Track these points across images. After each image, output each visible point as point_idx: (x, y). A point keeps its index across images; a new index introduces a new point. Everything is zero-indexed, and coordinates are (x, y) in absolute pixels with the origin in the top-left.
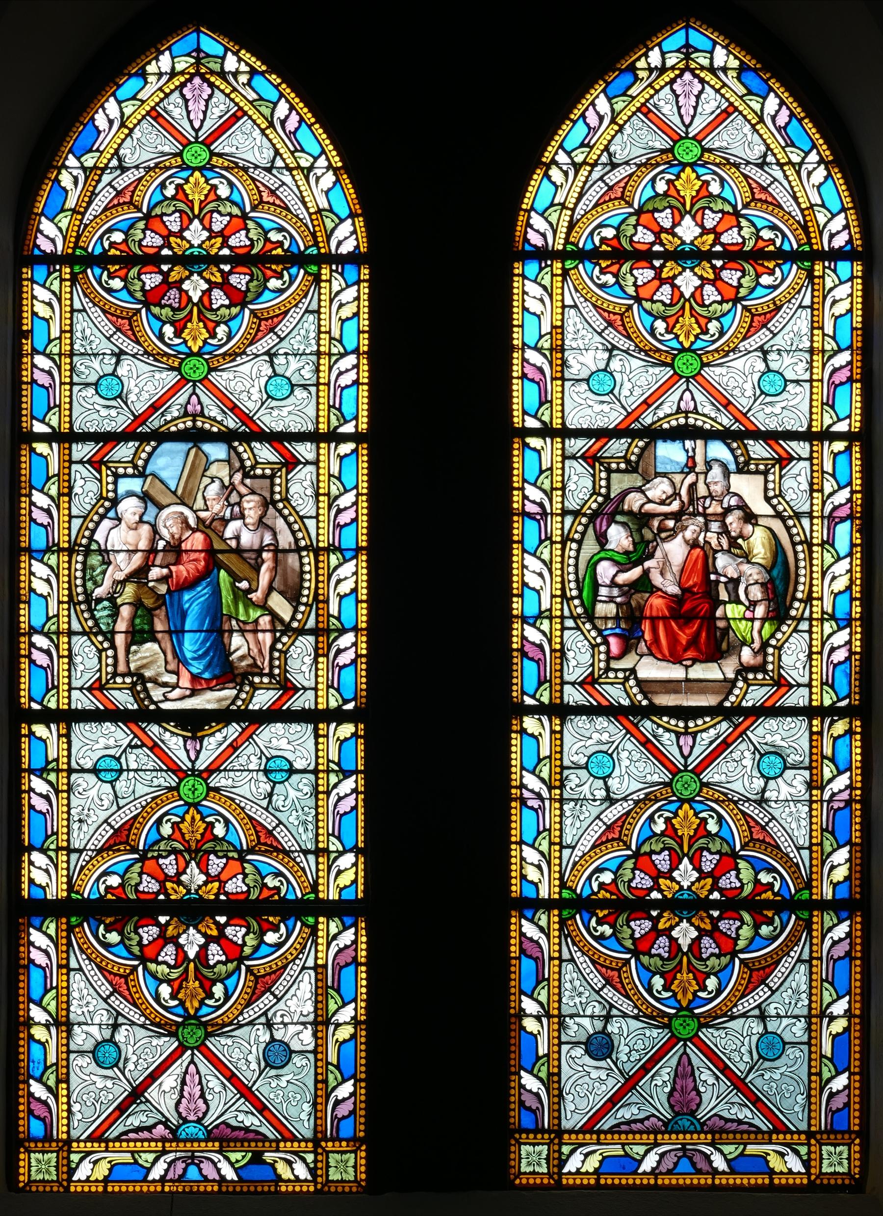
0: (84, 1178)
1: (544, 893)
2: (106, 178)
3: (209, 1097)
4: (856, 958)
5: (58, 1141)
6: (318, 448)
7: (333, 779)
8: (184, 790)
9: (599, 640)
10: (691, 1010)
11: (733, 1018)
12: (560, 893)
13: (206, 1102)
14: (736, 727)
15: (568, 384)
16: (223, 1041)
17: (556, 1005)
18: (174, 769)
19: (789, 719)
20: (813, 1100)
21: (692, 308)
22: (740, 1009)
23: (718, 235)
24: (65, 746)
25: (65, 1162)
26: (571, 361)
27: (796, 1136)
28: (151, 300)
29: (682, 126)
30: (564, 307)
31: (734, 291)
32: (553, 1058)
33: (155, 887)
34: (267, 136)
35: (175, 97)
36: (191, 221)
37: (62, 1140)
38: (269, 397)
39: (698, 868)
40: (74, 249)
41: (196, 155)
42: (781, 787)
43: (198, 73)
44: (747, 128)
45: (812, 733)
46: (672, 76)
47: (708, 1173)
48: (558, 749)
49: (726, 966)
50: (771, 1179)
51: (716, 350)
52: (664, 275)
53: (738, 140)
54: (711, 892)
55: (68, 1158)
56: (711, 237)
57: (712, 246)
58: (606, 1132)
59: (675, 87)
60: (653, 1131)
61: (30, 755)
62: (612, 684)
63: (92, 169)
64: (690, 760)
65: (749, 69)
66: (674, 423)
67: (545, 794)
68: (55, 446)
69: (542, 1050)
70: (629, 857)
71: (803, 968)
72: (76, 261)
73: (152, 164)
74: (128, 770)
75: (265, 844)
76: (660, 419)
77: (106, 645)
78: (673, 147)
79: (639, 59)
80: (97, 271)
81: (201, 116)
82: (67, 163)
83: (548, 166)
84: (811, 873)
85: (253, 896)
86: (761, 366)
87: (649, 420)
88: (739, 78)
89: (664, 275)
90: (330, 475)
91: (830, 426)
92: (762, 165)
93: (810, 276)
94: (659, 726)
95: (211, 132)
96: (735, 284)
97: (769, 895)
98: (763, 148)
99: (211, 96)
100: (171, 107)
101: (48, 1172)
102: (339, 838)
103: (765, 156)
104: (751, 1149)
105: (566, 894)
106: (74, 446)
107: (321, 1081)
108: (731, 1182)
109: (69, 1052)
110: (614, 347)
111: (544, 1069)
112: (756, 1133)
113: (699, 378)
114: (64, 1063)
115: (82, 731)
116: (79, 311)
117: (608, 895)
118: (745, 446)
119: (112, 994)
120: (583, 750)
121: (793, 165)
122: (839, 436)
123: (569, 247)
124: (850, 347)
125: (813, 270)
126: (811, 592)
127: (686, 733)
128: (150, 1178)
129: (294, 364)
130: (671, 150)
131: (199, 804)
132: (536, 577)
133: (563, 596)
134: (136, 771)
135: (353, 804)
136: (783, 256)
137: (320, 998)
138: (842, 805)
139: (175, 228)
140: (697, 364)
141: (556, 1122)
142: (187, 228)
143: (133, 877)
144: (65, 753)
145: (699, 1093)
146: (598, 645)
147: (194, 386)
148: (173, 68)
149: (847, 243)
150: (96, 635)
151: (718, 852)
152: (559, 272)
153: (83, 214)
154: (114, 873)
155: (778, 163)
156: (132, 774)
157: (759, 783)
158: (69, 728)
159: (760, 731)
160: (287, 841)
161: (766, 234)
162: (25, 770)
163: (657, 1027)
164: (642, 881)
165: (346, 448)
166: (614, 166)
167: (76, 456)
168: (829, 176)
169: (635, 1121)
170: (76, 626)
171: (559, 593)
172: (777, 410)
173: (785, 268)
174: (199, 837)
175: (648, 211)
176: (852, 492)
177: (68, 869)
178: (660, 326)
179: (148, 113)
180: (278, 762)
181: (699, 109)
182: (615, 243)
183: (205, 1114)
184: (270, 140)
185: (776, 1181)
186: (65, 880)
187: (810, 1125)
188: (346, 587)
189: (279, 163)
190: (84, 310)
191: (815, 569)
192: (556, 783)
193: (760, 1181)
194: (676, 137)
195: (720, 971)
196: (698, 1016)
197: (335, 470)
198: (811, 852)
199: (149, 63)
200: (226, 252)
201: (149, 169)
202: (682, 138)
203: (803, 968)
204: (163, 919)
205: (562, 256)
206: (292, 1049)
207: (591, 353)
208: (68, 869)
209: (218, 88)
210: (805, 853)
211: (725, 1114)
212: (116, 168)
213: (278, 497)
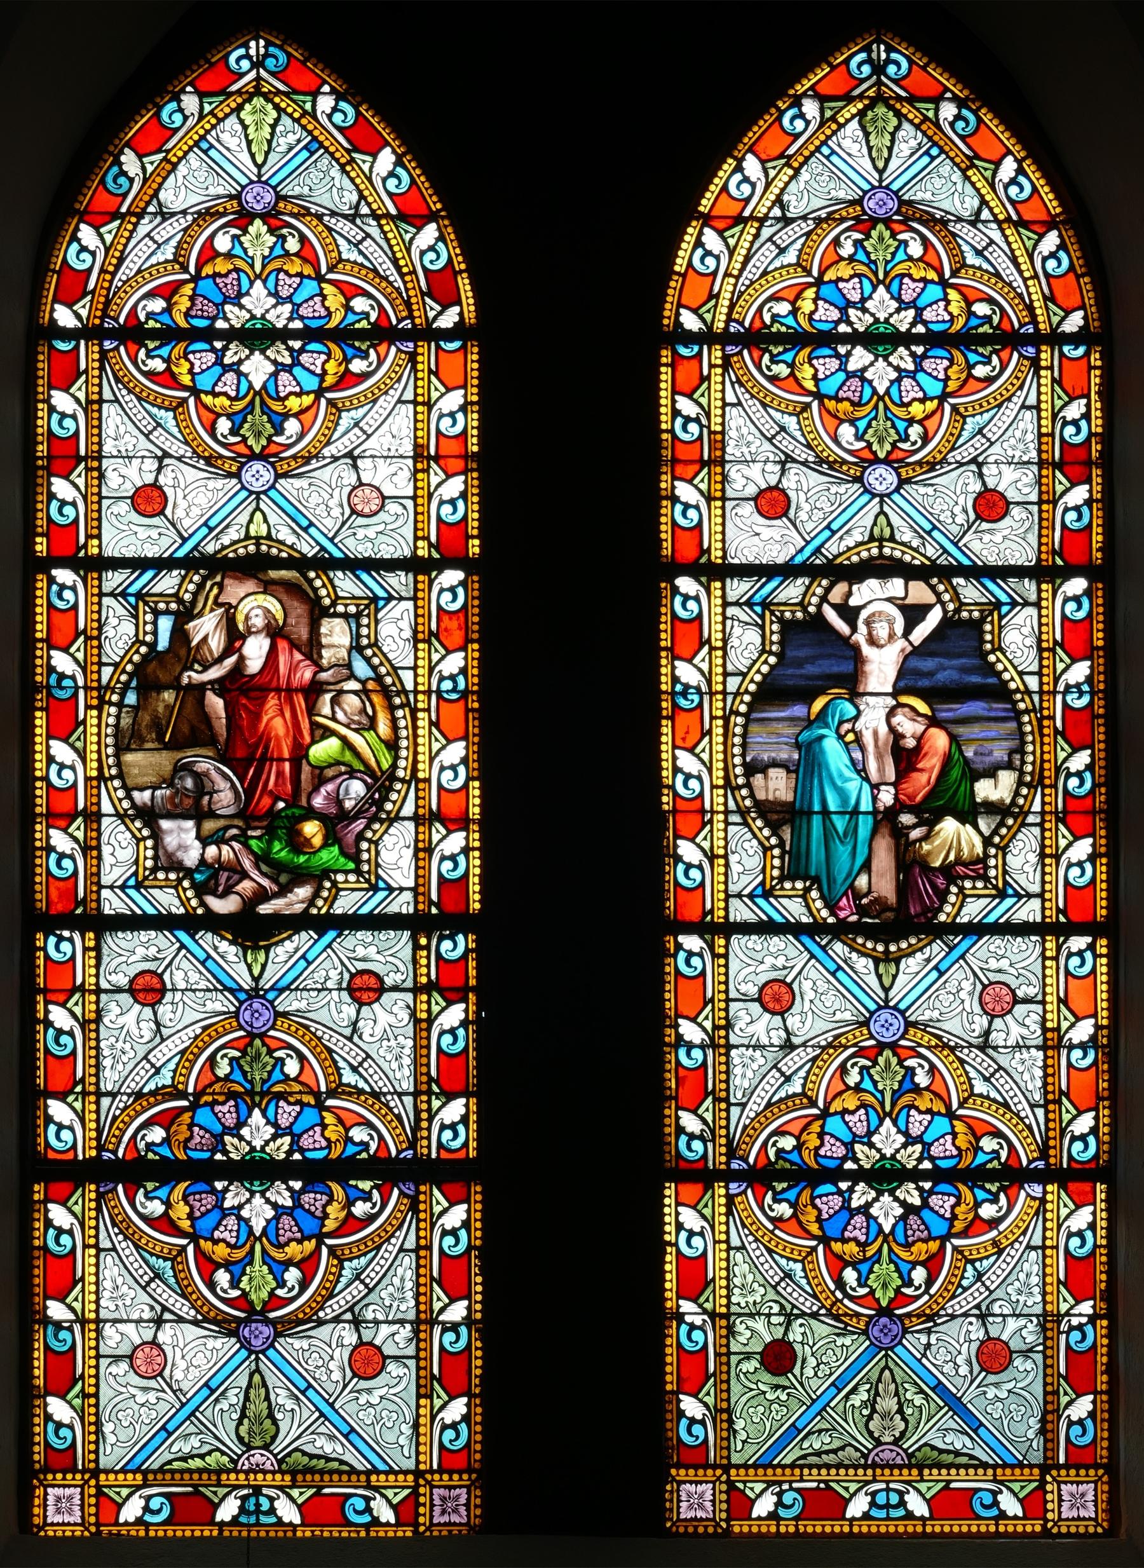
3: (279, 1416)
11: (321, 1323)
13: (904, 1419)
15: (729, 505)
17: (93, 1307)
20: (422, 1430)
21: (886, 408)
22: (327, 1313)
26: (733, 474)
30: (725, 405)
38: (353, 511)
40: (102, 318)
52: (227, 361)
56: (911, 313)
58: (155, 1472)
71: (408, 1261)
73: (823, 214)
74: (174, 990)
76: (224, 548)
77: (145, 832)
87: (210, 549)
89: (227, 361)
95: (259, 174)
98: (355, 197)
99: (897, 128)
101: (701, 1506)
103: (979, 212)
107: (1051, 1394)
109: (98, 1357)
110: (166, 455)
112: (349, 1473)
113: (272, 493)
114: (93, 1371)
115: (118, 943)
116: (733, 405)
118: (331, 581)
119: (152, 1280)
120: (752, 977)
126: (415, 770)
129: (1009, 474)
137: (422, 1290)
141: (92, 1457)
145: (275, 1422)
146: (772, 847)
147: (258, 499)
153: (113, 274)
155: (996, 220)
156: (179, 995)
157: (982, 1022)
159: (983, 954)
169: (827, 1452)
181: (895, 150)
183: (274, 1438)
184: (787, 184)
187: (418, 1462)
189: (365, 210)
190: (740, 404)
201: (819, 221)
204: (219, 1185)
211: (308, 1449)
212: (155, 214)
213: (365, 642)
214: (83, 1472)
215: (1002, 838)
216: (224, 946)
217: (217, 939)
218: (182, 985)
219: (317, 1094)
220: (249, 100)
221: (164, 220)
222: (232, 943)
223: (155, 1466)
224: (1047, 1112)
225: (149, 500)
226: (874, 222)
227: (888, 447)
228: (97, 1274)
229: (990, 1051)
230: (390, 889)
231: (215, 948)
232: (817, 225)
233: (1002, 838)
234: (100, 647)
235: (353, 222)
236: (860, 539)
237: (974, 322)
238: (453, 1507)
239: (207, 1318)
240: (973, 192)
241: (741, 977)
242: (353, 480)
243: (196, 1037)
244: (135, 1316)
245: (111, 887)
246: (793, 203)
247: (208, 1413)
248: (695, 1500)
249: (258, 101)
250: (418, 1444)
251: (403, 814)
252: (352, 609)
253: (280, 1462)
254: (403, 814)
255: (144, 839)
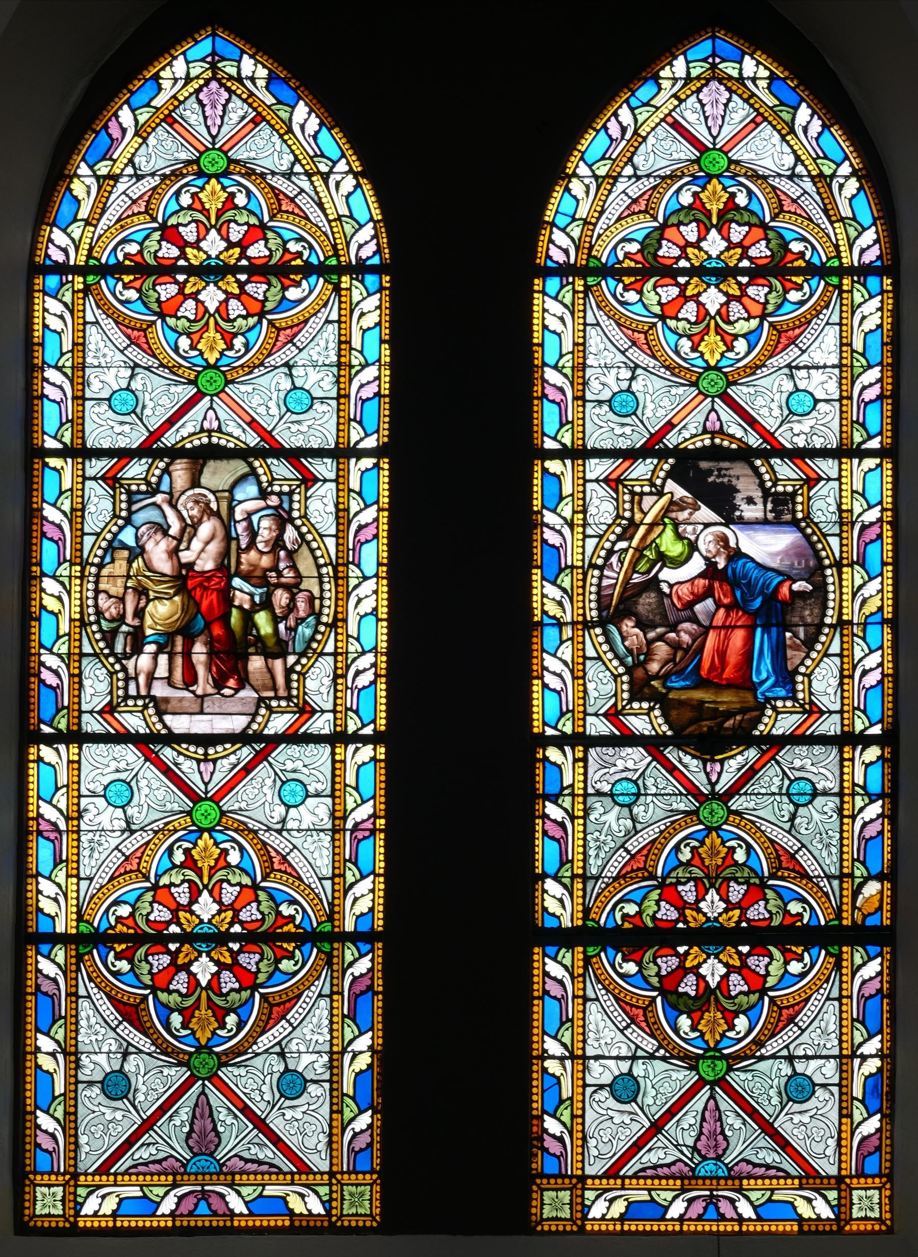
0: (599, 1216)
1: (60, 928)
2: (121, 187)
3: (221, 1129)
4: (378, 993)
5: (571, 1177)
6: (840, 463)
7: (859, 802)
8: (704, 813)
9: (117, 667)
10: (210, 1048)
12: (77, 927)
14: (764, 753)
16: (236, 1071)
18: (692, 791)
19: (102, 745)
21: (216, 323)
23: (745, 250)
24: (581, 771)
25: (579, 1200)
27: (318, 1177)
28: (667, 313)
29: (697, 132)
31: (760, 307)
32: (71, 1097)
33: (673, 915)
34: (787, 142)
35: (192, 103)
36: (208, 231)
37: (577, 1177)
38: (791, 412)
39: (725, 899)
41: (214, 162)
42: (812, 812)
43: (214, 78)
44: (777, 137)
45: (334, 761)
46: (196, 86)
47: (224, 1215)
48: (76, 779)
49: (247, 1001)
50: (292, 1221)
51: (242, 366)
53: (265, 150)
54: (231, 924)
55: (582, 1196)
57: (238, 260)
58: (630, 1178)
59: (701, 96)
60: (175, 1173)
61: (544, 781)
62: (635, 715)
63: (604, 178)
64: (210, 787)
65: (779, 78)
66: (197, 443)
67: (62, 826)
68: (568, 462)
69: (59, 1089)
70: (148, 889)
72: (586, 271)
73: (167, 171)
75: (787, 869)
78: (199, 158)
79: (163, 69)
80: (111, 281)
81: (218, 122)
82: (79, 172)
83: (570, 177)
84: (842, 903)
85: (776, 922)
86: (286, 384)
88: (267, 88)
90: (853, 492)
91: (357, 443)
92: (288, 175)
93: (337, 289)
94: (179, 753)
95: (224, 139)
96: (261, 297)
97: (290, 928)
98: (292, 158)
99: (228, 101)
100: (188, 113)
102: (863, 863)
104: (270, 1191)
105: (83, 928)
106: (87, 463)
108: (250, 1224)
110: (137, 365)
111: (60, 1109)
113: (222, 395)
117: (125, 929)
118: (771, 467)
121: (825, 177)
122: (367, 453)
123: (92, 262)
124: (881, 364)
125: (340, 282)
127: (206, 760)
128: (668, 1216)
129: (314, 376)
130: (197, 162)
131: (719, 828)
132: (57, 599)
133: (81, 620)
134: (655, 795)
135: (879, 828)
136: (308, 270)
138: (367, 834)
139: (692, 238)
140: (221, 381)
142: (705, 239)
143: (145, 908)
144: (581, 778)
145: (218, 1134)
146: (117, 672)
148: (188, 73)
149: (878, 258)
150: (107, 657)
151: (747, 882)
152: (81, 286)
154: (125, 902)
156: (649, 798)
158: (586, 752)
160: (812, 869)
161: (293, 247)
162: (540, 796)
163: (177, 1065)
164: (161, 914)
165: (870, 462)
166: (139, 178)
167: (90, 472)
168: (358, 186)
169: (662, 1166)
170: (87, 649)
171: (78, 616)
172: (304, 428)
173: (813, 283)
174: (720, 862)
175: (673, 225)
176: (883, 510)
177: (78, 898)
178: (184, 343)
179: (663, 120)
180: (802, 784)
181: (727, 119)
182: (138, 259)
184: (791, 147)
185: (297, 1223)
186: (74, 909)
187: (840, 1169)
188: (367, 606)
190: (97, 322)
191: (845, 590)
192: (75, 815)
193: (280, 1223)
194: (202, 148)
195: (241, 1006)
196: (217, 1054)
197: (858, 486)
198: (841, 882)
199: (663, 68)
200: (745, 263)
201: (164, 177)
202: (207, 149)
203: (324, 1003)
204: (681, 950)
205: (341, 270)
206: (307, 1085)
207: (113, 371)
208: (78, 898)
209: (234, 92)
210: (328, 884)
211: (246, 1155)
214: (64, 1174)
215: (303, 666)
216: (687, 759)
217: (681, 754)
218: (653, 790)
219: (762, 878)
220: (706, 85)
221: (138, 180)
222: (694, 757)
223: (630, 1173)
224: (334, 884)
225: (624, 404)
226: (710, 177)
227: (717, 356)
228: (584, 1019)
229: (285, 833)
230: (822, 713)
231: (680, 761)
232: (162, 180)
233: (303, 666)
234: (83, 517)
235: (289, 179)
236: (192, 430)
237: (288, 257)
238: (361, 1202)
239: (674, 1054)
240: (789, 150)
241: (90, 778)
242: (289, 386)
243: (661, 832)
244: (614, 1053)
245: (91, 712)
246: (144, 163)
247: (164, 1128)
248: (554, 1205)
249: (714, 85)
250: (840, 1154)
251: (831, 651)
252: (286, 489)
253: (730, 1170)
254: (831, 651)
255: (621, 675)
